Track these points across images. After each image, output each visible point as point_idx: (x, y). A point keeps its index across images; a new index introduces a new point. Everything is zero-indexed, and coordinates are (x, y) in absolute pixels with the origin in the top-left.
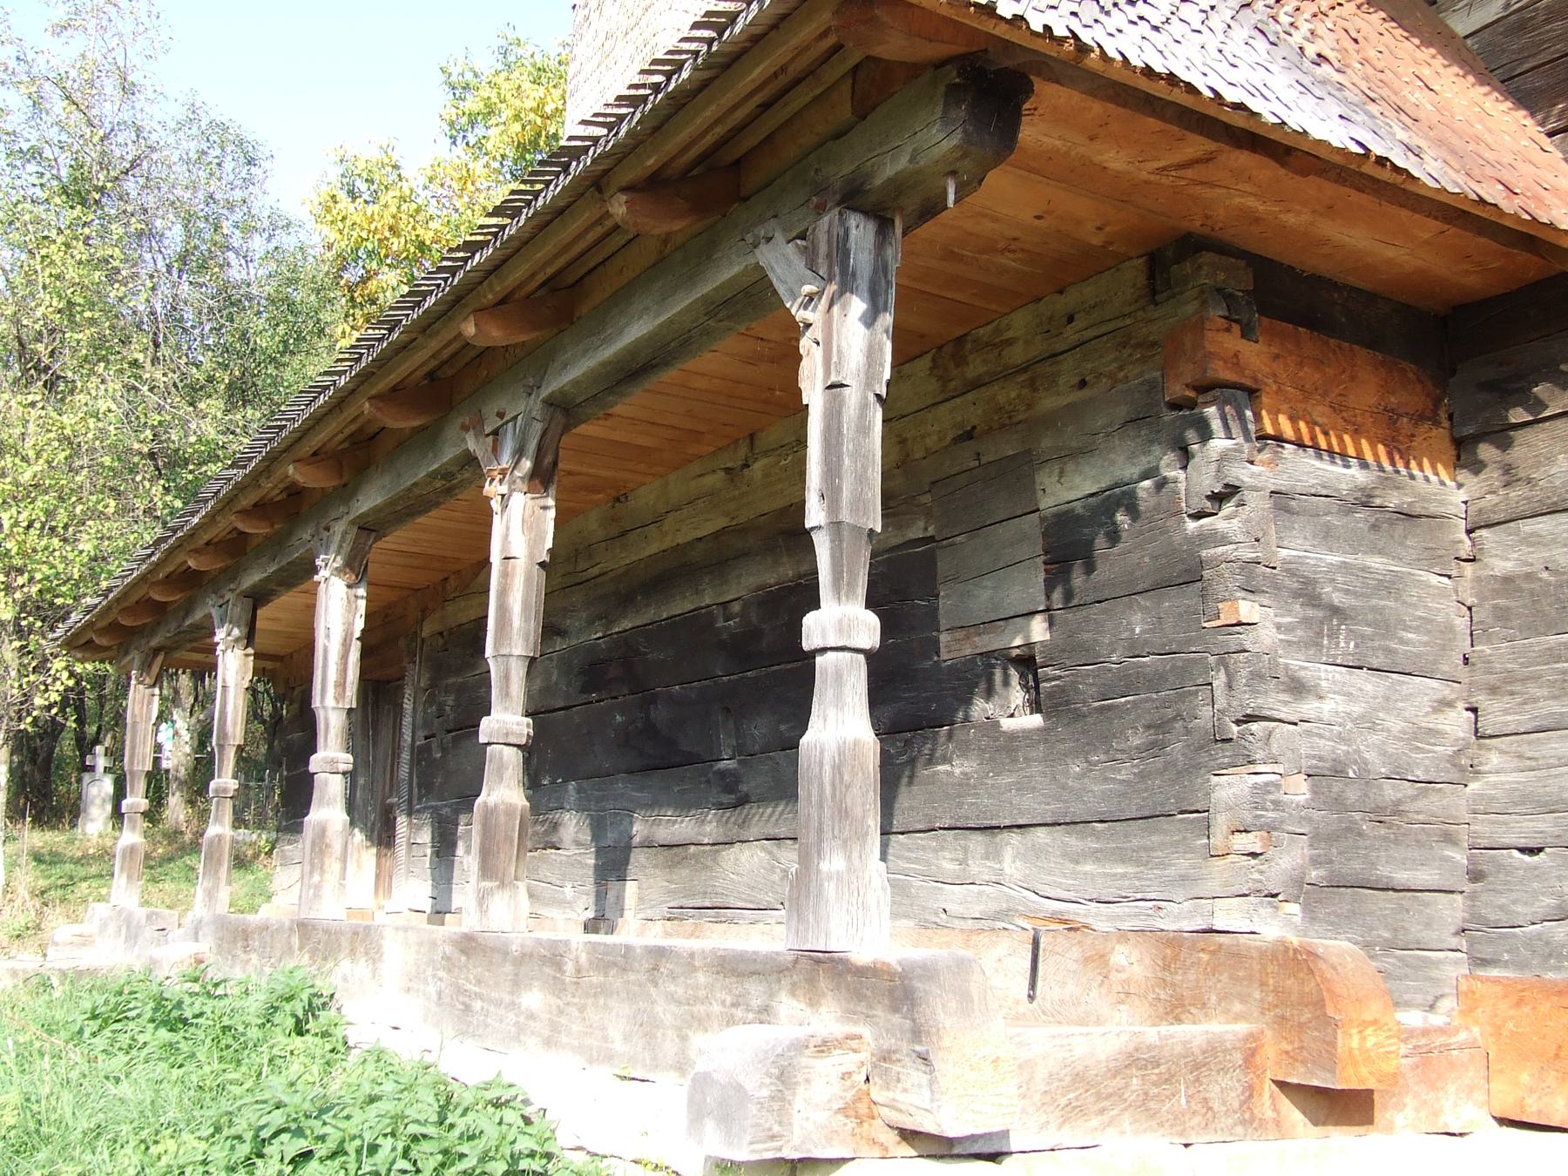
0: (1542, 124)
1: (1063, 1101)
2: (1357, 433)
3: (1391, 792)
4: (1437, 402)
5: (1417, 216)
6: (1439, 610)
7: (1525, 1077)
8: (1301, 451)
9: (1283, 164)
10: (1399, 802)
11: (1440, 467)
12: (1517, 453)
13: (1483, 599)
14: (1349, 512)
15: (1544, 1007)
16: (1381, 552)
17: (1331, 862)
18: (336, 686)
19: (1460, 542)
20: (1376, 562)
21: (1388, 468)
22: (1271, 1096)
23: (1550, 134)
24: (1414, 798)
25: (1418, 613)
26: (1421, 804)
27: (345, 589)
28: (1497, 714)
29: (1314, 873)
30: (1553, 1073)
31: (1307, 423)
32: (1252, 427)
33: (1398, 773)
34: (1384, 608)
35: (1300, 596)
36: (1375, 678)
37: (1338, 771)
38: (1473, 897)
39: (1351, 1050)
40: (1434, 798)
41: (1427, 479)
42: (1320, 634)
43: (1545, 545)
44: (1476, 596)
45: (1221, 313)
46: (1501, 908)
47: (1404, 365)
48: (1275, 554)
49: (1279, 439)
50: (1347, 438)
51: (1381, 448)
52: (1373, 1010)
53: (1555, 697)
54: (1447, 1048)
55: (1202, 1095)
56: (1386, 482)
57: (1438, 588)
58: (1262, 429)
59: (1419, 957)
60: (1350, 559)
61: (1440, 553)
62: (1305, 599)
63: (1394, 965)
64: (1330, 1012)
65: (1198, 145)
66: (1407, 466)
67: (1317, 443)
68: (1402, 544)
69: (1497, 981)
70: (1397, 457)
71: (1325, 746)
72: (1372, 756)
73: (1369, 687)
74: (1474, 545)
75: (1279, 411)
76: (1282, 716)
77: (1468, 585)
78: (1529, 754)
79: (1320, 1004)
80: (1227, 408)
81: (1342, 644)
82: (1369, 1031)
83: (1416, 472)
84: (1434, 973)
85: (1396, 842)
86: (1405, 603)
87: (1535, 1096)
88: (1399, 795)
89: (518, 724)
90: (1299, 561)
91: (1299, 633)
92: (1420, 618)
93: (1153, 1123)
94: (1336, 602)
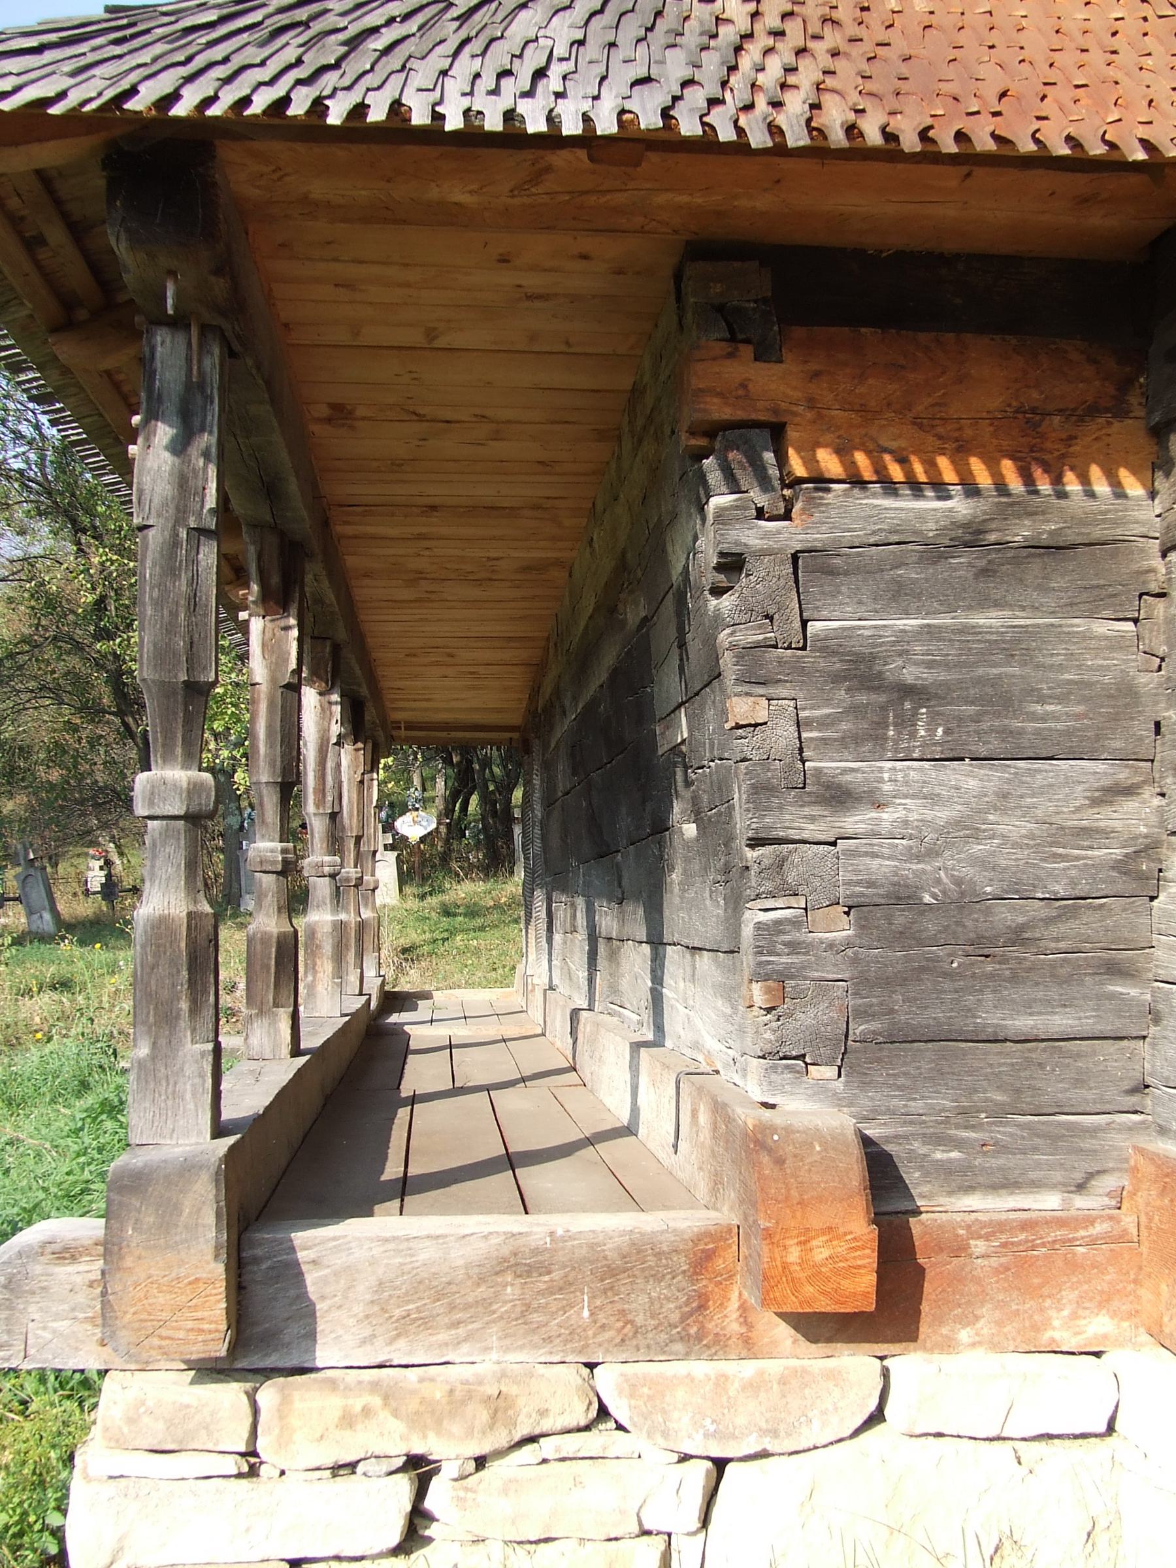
1: (398, 1312)
2: (960, 451)
3: (1006, 915)
8: (856, 491)
14: (942, 557)
16: (998, 605)
17: (891, 1011)
18: (315, 793)
19: (1152, 570)
20: (988, 620)
22: (744, 1308)
24: (1049, 921)
25: (1067, 676)
27: (318, 697)
31: (868, 453)
32: (774, 472)
33: (1017, 892)
35: (845, 678)
36: (983, 770)
40: (1088, 917)
45: (717, 335)
54: (1069, 1242)
55: (619, 1306)
56: (1010, 508)
57: (1107, 638)
59: (1060, 1124)
62: (855, 682)
63: (1011, 1135)
66: (1057, 480)
67: (888, 476)
71: (880, 868)
76: (806, 835)
80: (732, 455)
84: (1088, 1144)
85: (1015, 979)
86: (1038, 666)
88: (1021, 920)
89: (272, 851)
90: (847, 633)
93: (536, 1338)
94: (910, 680)
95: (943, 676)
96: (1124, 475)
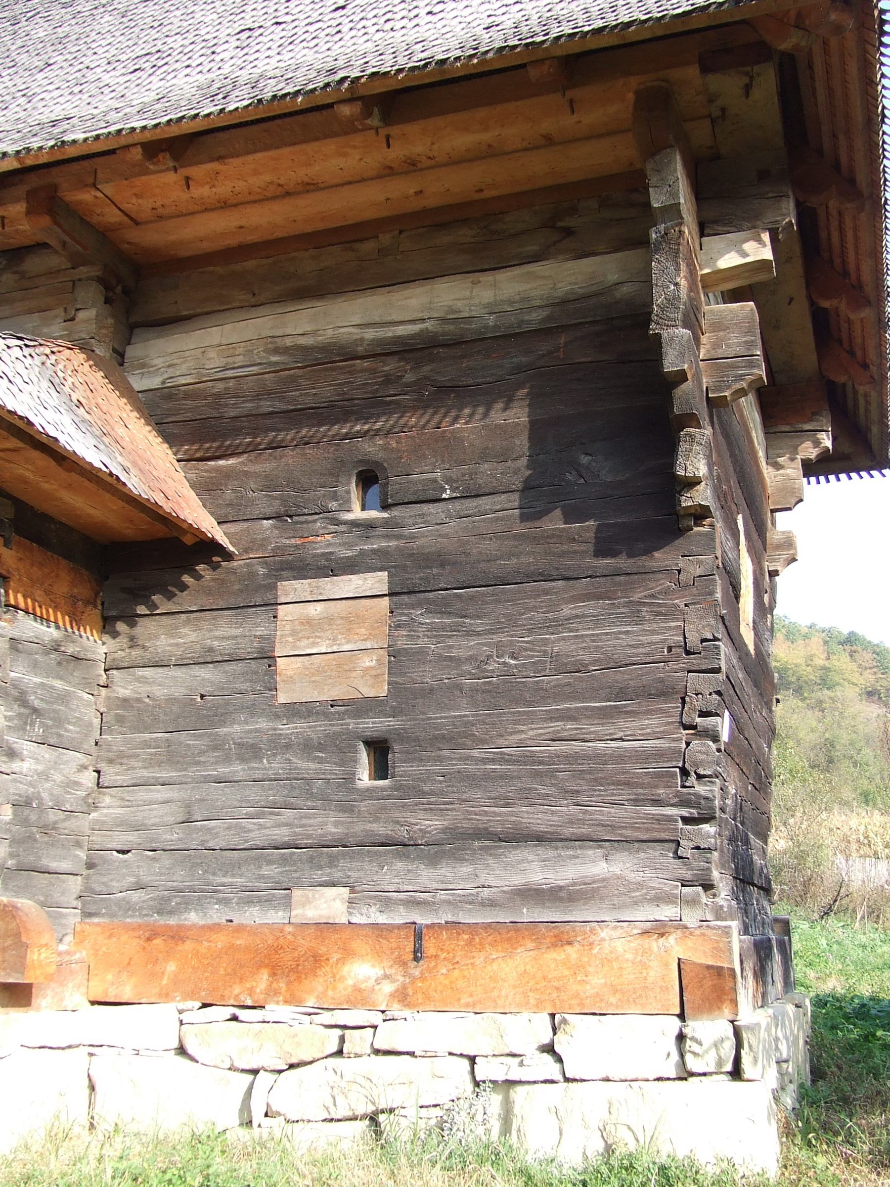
0: (175, 454)
2: (56, 609)
3: (53, 816)
4: (97, 594)
5: (114, 498)
6: (86, 714)
7: (110, 977)
9: (60, 465)
10: (56, 823)
11: (94, 632)
12: (138, 630)
13: (110, 710)
15: (124, 938)
16: (61, 678)
17: (19, 856)
19: (101, 675)
20: (58, 684)
21: (70, 630)
23: (178, 461)
26: (67, 824)
28: (111, 775)
29: (10, 862)
30: (125, 973)
34: (60, 710)
37: (28, 803)
38: (88, 878)
39: (33, 960)
40: (73, 820)
41: (88, 638)
42: (26, 723)
43: (149, 684)
44: (106, 707)
46: (104, 884)
47: (83, 571)
48: (8, 674)
49: (16, 607)
50: (51, 611)
51: (67, 618)
52: (46, 938)
53: (145, 768)
56: (68, 638)
58: (8, 601)
60: (45, 681)
61: (89, 681)
64: (24, 939)
65: (14, 443)
68: (72, 674)
69: (98, 924)
70: (74, 624)
72: (45, 795)
73: (47, 756)
74: (108, 678)
75: (18, 592)
77: (102, 700)
78: (128, 798)
79: (18, 935)
81: (36, 730)
82: (43, 950)
83: (83, 634)
84: (64, 921)
86: (70, 708)
87: (115, 987)
90: (20, 680)
91: (16, 722)
92: (77, 717)
95: (45, 706)
96: (94, 632)
